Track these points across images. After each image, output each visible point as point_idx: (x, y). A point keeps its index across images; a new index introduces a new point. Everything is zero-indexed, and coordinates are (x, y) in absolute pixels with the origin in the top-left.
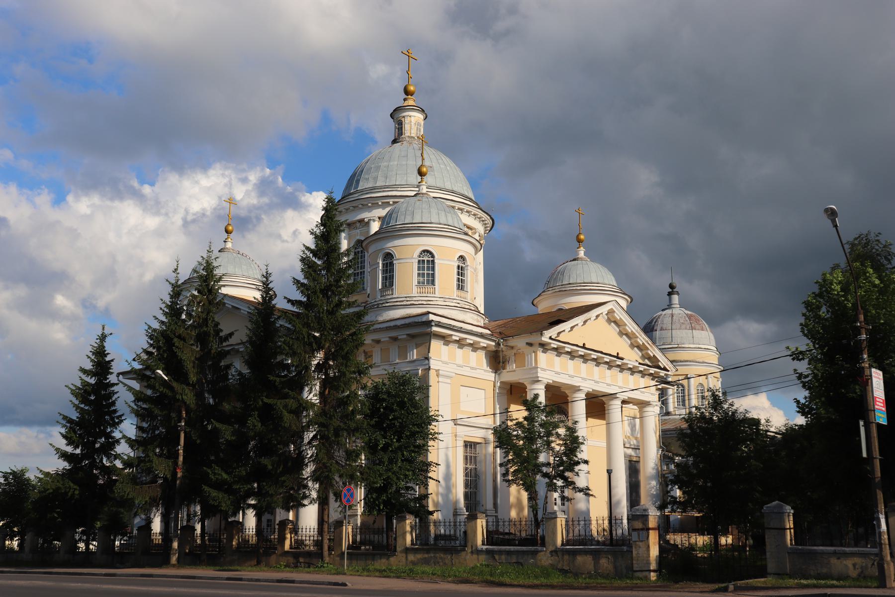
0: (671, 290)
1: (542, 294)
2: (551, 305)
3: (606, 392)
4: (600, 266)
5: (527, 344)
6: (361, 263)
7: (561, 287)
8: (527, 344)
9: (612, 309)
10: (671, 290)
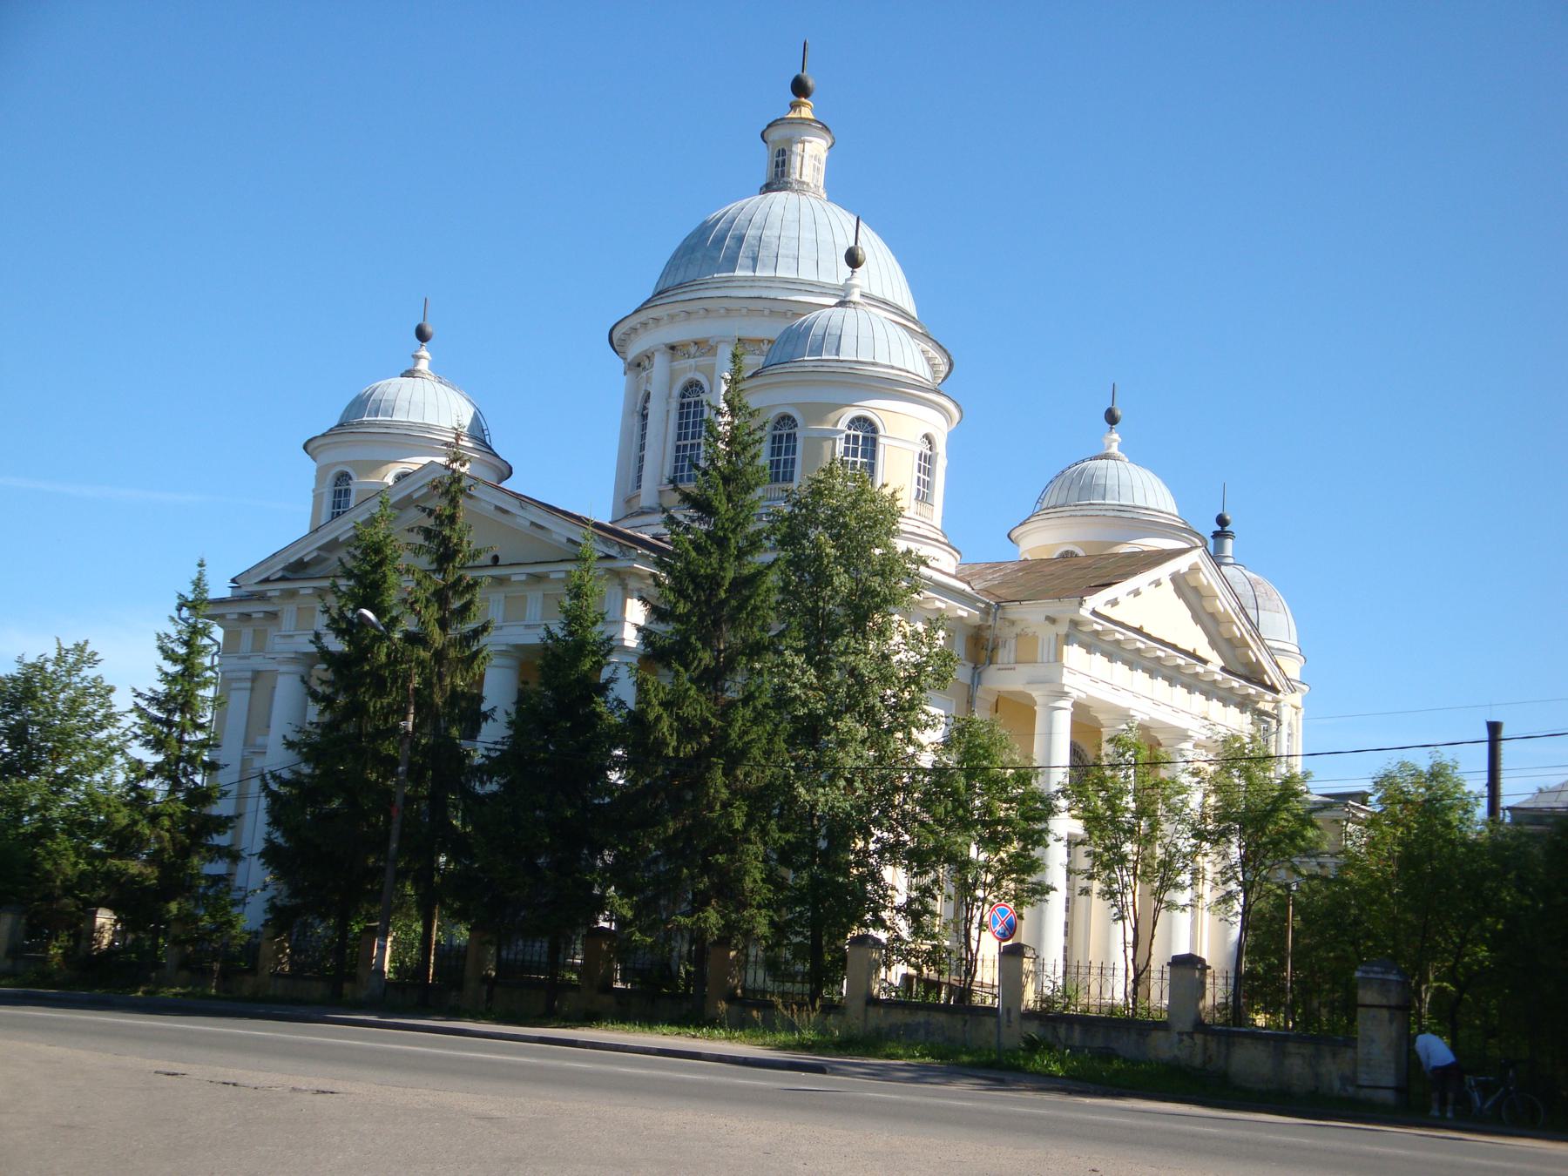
0: (1219, 528)
3: (1160, 719)
4: (1151, 475)
6: (687, 424)
7: (1074, 508)
9: (1196, 563)
10: (1219, 528)
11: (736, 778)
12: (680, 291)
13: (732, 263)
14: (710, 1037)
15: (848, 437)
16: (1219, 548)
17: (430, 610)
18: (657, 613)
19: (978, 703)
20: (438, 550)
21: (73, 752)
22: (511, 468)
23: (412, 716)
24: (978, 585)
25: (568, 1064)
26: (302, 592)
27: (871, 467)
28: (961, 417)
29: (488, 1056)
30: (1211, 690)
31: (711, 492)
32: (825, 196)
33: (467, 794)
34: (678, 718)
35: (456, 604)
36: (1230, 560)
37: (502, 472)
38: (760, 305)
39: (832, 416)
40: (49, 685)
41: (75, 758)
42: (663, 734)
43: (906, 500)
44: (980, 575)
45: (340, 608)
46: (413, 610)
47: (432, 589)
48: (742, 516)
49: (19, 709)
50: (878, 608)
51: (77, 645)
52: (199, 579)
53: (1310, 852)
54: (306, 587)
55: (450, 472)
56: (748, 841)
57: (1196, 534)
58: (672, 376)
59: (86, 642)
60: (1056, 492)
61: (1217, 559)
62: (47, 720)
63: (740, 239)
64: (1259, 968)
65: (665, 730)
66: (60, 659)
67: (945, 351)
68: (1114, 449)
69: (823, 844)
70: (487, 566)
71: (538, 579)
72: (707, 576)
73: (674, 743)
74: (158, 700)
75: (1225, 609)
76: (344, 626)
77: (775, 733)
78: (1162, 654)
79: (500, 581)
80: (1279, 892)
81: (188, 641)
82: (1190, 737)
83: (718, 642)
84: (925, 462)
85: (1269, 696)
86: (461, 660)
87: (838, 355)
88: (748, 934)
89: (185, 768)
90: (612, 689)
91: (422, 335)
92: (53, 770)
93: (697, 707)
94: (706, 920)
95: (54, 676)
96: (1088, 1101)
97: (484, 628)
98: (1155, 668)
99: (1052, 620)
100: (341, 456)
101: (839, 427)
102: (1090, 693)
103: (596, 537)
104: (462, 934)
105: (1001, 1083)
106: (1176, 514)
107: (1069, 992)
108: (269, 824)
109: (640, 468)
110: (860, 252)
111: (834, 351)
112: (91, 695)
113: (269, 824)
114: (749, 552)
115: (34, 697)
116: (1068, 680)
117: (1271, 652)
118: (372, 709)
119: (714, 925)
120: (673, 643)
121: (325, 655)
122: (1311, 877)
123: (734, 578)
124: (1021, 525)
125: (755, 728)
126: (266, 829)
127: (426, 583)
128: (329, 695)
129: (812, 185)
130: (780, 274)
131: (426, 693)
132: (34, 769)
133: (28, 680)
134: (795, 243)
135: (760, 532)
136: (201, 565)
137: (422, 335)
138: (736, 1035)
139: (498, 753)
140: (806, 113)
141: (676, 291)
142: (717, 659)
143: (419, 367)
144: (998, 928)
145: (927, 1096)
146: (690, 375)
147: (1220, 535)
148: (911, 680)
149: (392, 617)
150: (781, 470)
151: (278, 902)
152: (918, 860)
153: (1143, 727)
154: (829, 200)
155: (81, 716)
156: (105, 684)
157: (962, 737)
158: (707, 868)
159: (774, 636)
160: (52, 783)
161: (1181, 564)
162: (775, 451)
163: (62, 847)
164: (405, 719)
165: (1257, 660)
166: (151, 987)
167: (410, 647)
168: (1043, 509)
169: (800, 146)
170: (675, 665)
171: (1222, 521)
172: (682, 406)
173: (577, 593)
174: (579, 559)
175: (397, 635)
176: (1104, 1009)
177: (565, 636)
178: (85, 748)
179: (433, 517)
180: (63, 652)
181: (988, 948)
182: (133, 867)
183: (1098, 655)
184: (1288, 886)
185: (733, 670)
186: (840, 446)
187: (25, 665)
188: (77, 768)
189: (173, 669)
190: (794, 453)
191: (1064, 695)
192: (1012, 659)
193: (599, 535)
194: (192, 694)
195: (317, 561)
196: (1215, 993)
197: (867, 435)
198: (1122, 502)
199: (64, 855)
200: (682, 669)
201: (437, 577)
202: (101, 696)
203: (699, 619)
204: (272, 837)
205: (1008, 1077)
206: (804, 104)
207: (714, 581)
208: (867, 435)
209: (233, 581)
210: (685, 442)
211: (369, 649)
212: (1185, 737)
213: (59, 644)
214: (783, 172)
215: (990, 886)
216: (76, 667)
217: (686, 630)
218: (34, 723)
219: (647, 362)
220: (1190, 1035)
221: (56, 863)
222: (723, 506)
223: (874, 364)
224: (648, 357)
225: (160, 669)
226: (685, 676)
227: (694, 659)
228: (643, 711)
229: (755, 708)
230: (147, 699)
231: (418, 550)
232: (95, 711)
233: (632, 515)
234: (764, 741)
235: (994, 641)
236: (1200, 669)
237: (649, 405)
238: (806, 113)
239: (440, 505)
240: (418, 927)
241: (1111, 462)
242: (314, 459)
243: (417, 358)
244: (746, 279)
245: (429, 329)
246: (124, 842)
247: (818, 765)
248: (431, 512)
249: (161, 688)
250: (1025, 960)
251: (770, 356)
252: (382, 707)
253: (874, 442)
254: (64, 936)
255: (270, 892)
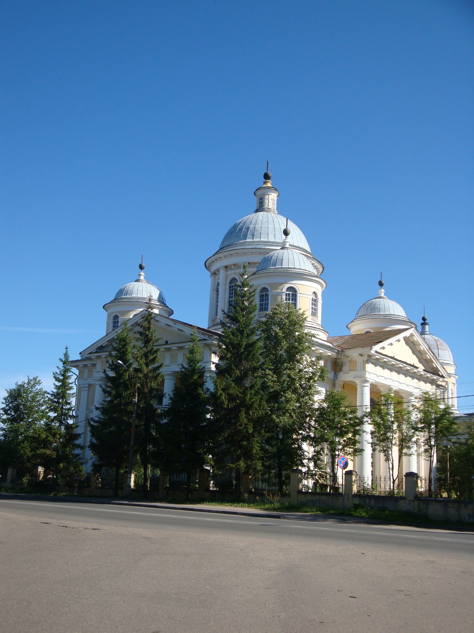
0: (423, 322)
1: (354, 321)
2: (362, 328)
4: (395, 303)
5: (360, 354)
8: (360, 354)
10: (423, 322)
11: (249, 414)
12: (228, 247)
13: (245, 237)
14: (242, 506)
15: (286, 294)
16: (423, 329)
17: (142, 360)
18: (221, 358)
19: (337, 385)
20: (145, 339)
21: (34, 414)
22: (173, 311)
23: (137, 397)
24: (335, 344)
25: (187, 517)
26: (103, 356)
27: (295, 304)
28: (326, 285)
29: (160, 515)
30: (420, 378)
31: (237, 315)
32: (277, 213)
33: (158, 424)
34: (228, 394)
35: (151, 357)
36: (428, 333)
37: (170, 312)
38: (255, 250)
39: (281, 287)
40: (25, 392)
41: (35, 416)
42: (223, 400)
43: (308, 314)
44: (336, 341)
45: (112, 361)
46: (137, 360)
47: (143, 353)
48: (248, 322)
49: (16, 400)
50: (297, 353)
51: (34, 378)
52: (66, 353)
53: (455, 433)
54: (104, 354)
55: (148, 312)
56: (254, 437)
57: (413, 323)
58: (226, 277)
59: (37, 377)
60: (363, 310)
61: (422, 333)
62: (25, 403)
63: (248, 229)
64: (443, 477)
65: (224, 398)
66: (29, 383)
67: (321, 263)
68: (382, 295)
69: (281, 437)
70: (163, 345)
71: (181, 348)
72: (237, 344)
73: (227, 403)
74: (54, 395)
75: (424, 349)
76: (114, 367)
77: (261, 399)
78: (402, 366)
79: (169, 350)
80: (444, 448)
81: (64, 374)
82: (414, 395)
83: (241, 367)
84: (314, 302)
85: (441, 379)
86: (153, 377)
87: (282, 266)
88: (255, 469)
89: (64, 418)
90: (205, 385)
91: (141, 267)
92: (28, 420)
93: (235, 390)
94: (240, 465)
95: (27, 389)
96: (374, 526)
97: (161, 366)
98: (399, 371)
99: (361, 355)
100: (115, 310)
101: (283, 291)
102: (399, 388)
103: (200, 333)
104: (158, 472)
105: (344, 521)
106: (405, 316)
107: (373, 487)
108: (91, 436)
109: (217, 309)
110: (288, 230)
111: (280, 265)
112: (39, 394)
113: (91, 436)
114: (251, 335)
115: (21, 396)
116: (368, 376)
117: (442, 364)
118: (124, 395)
119: (243, 467)
120: (226, 368)
121: (108, 378)
122: (454, 443)
123: (246, 344)
124: (351, 323)
125: (255, 397)
126: (90, 438)
127: (141, 351)
128: (110, 391)
129: (272, 209)
130: (261, 240)
131: (142, 389)
132: (22, 420)
133: (19, 390)
134: (267, 229)
135: (254, 328)
136: (66, 348)
137: (141, 267)
138: (251, 505)
139: (167, 409)
140: (269, 185)
141: (226, 248)
142: (241, 373)
143: (141, 278)
144: (342, 465)
145: (313, 526)
146: (233, 276)
147: (424, 324)
148: (311, 378)
149: (130, 363)
150: (264, 307)
151: (96, 463)
152: (315, 441)
153: (396, 392)
154: (279, 214)
155: (36, 402)
156: (43, 391)
157: (329, 397)
158: (241, 447)
159: (261, 365)
160: (28, 424)
161: (407, 334)
162: (261, 300)
163: (26, 445)
164: (135, 398)
165: (436, 366)
166: (56, 493)
167: (136, 373)
168: (358, 317)
169: (267, 196)
170: (227, 375)
171: (424, 319)
172: (230, 287)
173: (192, 352)
174: (193, 341)
175: (131, 369)
176: (387, 493)
177: (188, 367)
178: (38, 412)
179: (142, 328)
180: (30, 381)
181: (340, 473)
182: (48, 452)
183: (394, 372)
184: (446, 447)
185: (247, 376)
186: (284, 297)
187: (18, 385)
188: (35, 419)
189: (58, 384)
190: (268, 301)
191: (367, 381)
192: (348, 369)
193: (201, 332)
194: (65, 393)
195: (107, 346)
196: (422, 486)
197: (293, 293)
198: (386, 313)
199: (27, 448)
200: (229, 377)
201: (145, 349)
202: (42, 395)
203: (234, 359)
204: (92, 440)
205: (345, 518)
206: (268, 182)
207: (239, 345)
208: (293, 294)
209: (80, 354)
210: (232, 299)
211: (122, 374)
212: (411, 394)
213: (28, 378)
214: (262, 205)
215: (341, 450)
216: (34, 385)
217: (230, 363)
218: (21, 404)
219: (218, 273)
220: (413, 501)
221: (24, 451)
222: (241, 319)
223: (294, 268)
224: (218, 271)
225: (54, 384)
226: (230, 379)
227: (233, 373)
228: (216, 392)
229: (255, 390)
230: (51, 395)
231: (137, 340)
232: (40, 400)
233: (214, 325)
234: (258, 401)
235: (341, 363)
236: (415, 370)
237: (219, 287)
238: (269, 185)
239: (145, 324)
240: (142, 470)
241: (381, 299)
242: (107, 311)
243: (140, 275)
244: (250, 242)
245: (144, 265)
246: (46, 443)
247: (279, 409)
248: (142, 326)
249: (55, 391)
250: (353, 476)
251: (258, 267)
252: (127, 395)
253: (296, 295)
254: (28, 476)
255: (93, 460)
